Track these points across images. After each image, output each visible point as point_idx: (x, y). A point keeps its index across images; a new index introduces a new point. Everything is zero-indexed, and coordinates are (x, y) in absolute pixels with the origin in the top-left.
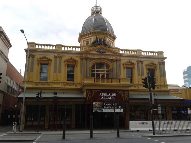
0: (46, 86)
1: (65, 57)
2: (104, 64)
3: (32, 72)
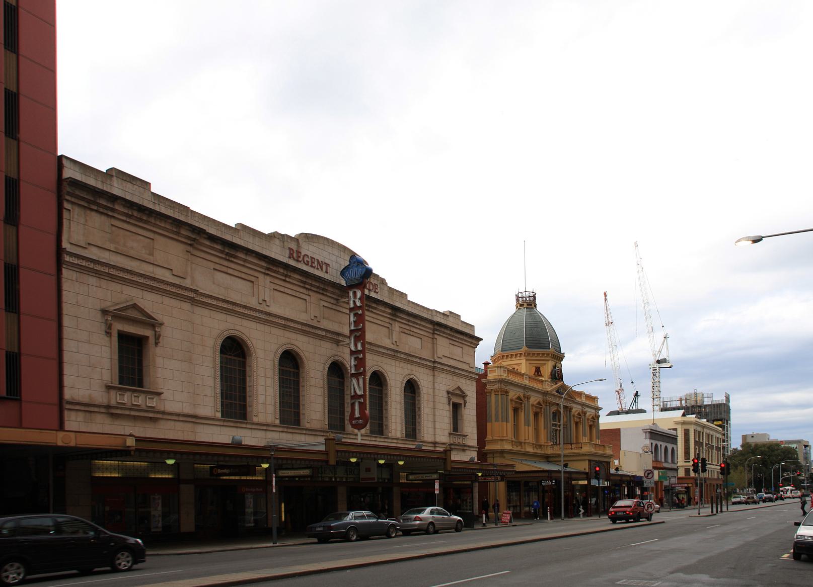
2: (620, 485)
3: (337, 461)
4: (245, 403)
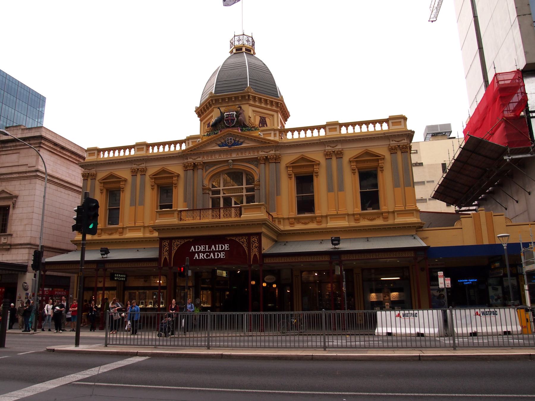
0: (116, 236)
1: (153, 169)
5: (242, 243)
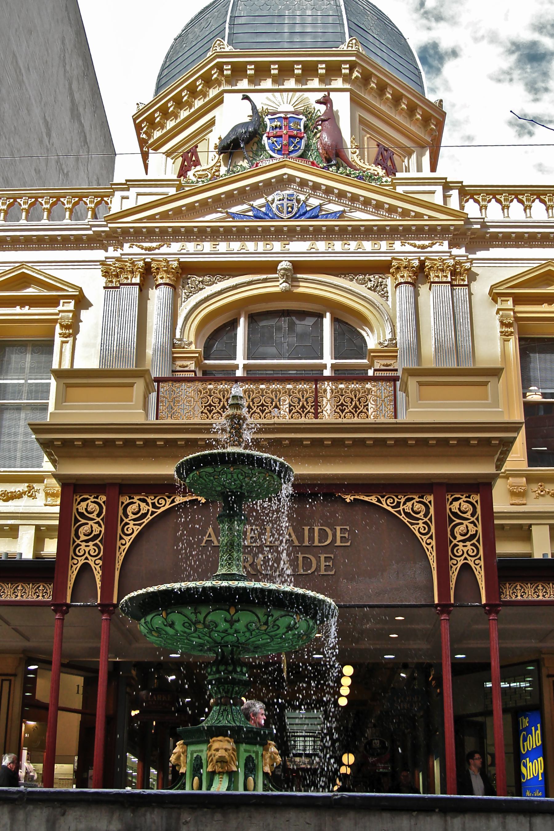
4: (27, 370)
5: (406, 520)
